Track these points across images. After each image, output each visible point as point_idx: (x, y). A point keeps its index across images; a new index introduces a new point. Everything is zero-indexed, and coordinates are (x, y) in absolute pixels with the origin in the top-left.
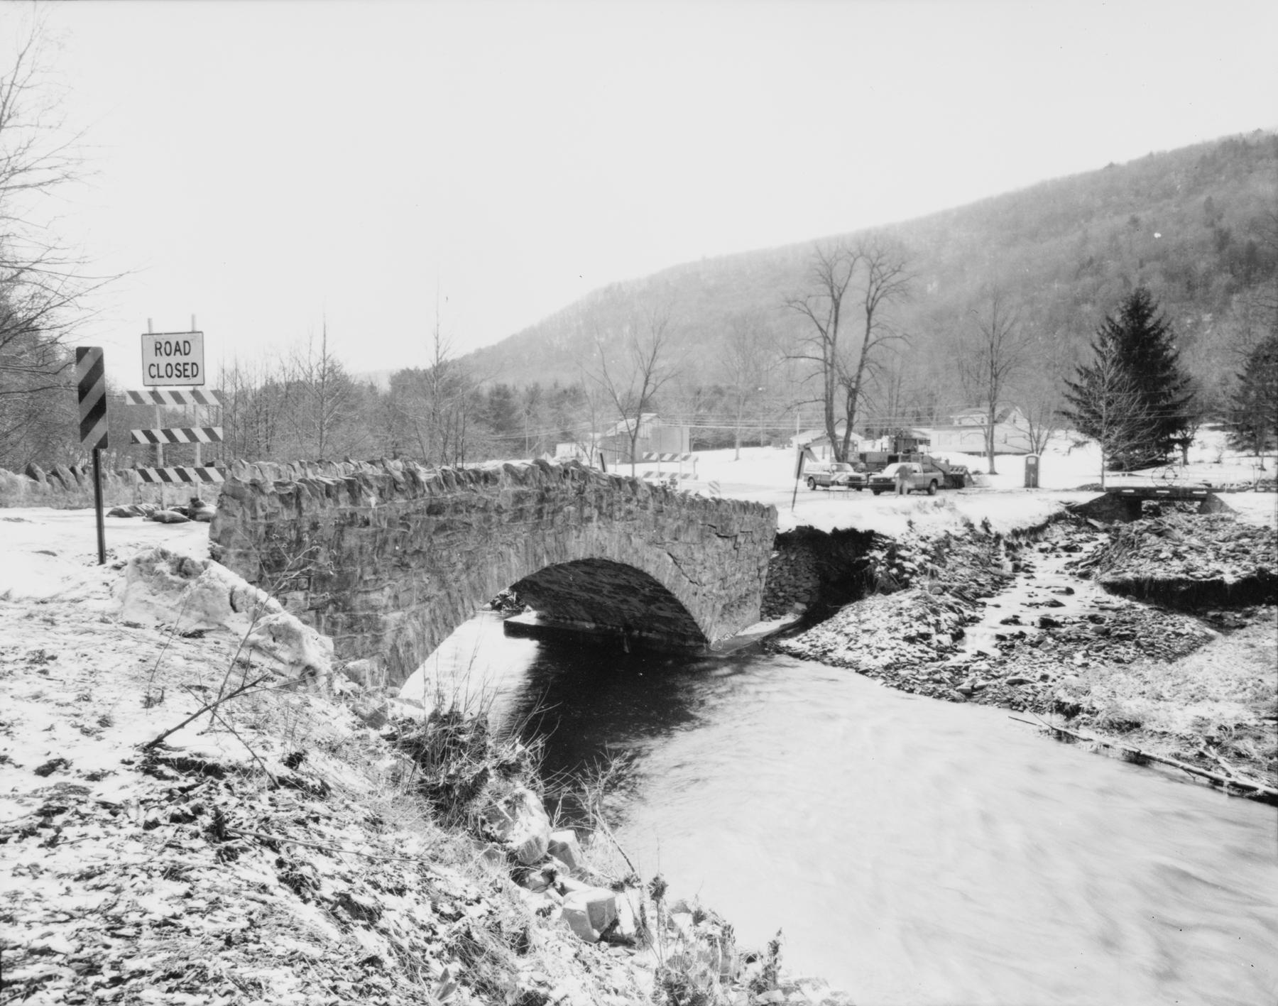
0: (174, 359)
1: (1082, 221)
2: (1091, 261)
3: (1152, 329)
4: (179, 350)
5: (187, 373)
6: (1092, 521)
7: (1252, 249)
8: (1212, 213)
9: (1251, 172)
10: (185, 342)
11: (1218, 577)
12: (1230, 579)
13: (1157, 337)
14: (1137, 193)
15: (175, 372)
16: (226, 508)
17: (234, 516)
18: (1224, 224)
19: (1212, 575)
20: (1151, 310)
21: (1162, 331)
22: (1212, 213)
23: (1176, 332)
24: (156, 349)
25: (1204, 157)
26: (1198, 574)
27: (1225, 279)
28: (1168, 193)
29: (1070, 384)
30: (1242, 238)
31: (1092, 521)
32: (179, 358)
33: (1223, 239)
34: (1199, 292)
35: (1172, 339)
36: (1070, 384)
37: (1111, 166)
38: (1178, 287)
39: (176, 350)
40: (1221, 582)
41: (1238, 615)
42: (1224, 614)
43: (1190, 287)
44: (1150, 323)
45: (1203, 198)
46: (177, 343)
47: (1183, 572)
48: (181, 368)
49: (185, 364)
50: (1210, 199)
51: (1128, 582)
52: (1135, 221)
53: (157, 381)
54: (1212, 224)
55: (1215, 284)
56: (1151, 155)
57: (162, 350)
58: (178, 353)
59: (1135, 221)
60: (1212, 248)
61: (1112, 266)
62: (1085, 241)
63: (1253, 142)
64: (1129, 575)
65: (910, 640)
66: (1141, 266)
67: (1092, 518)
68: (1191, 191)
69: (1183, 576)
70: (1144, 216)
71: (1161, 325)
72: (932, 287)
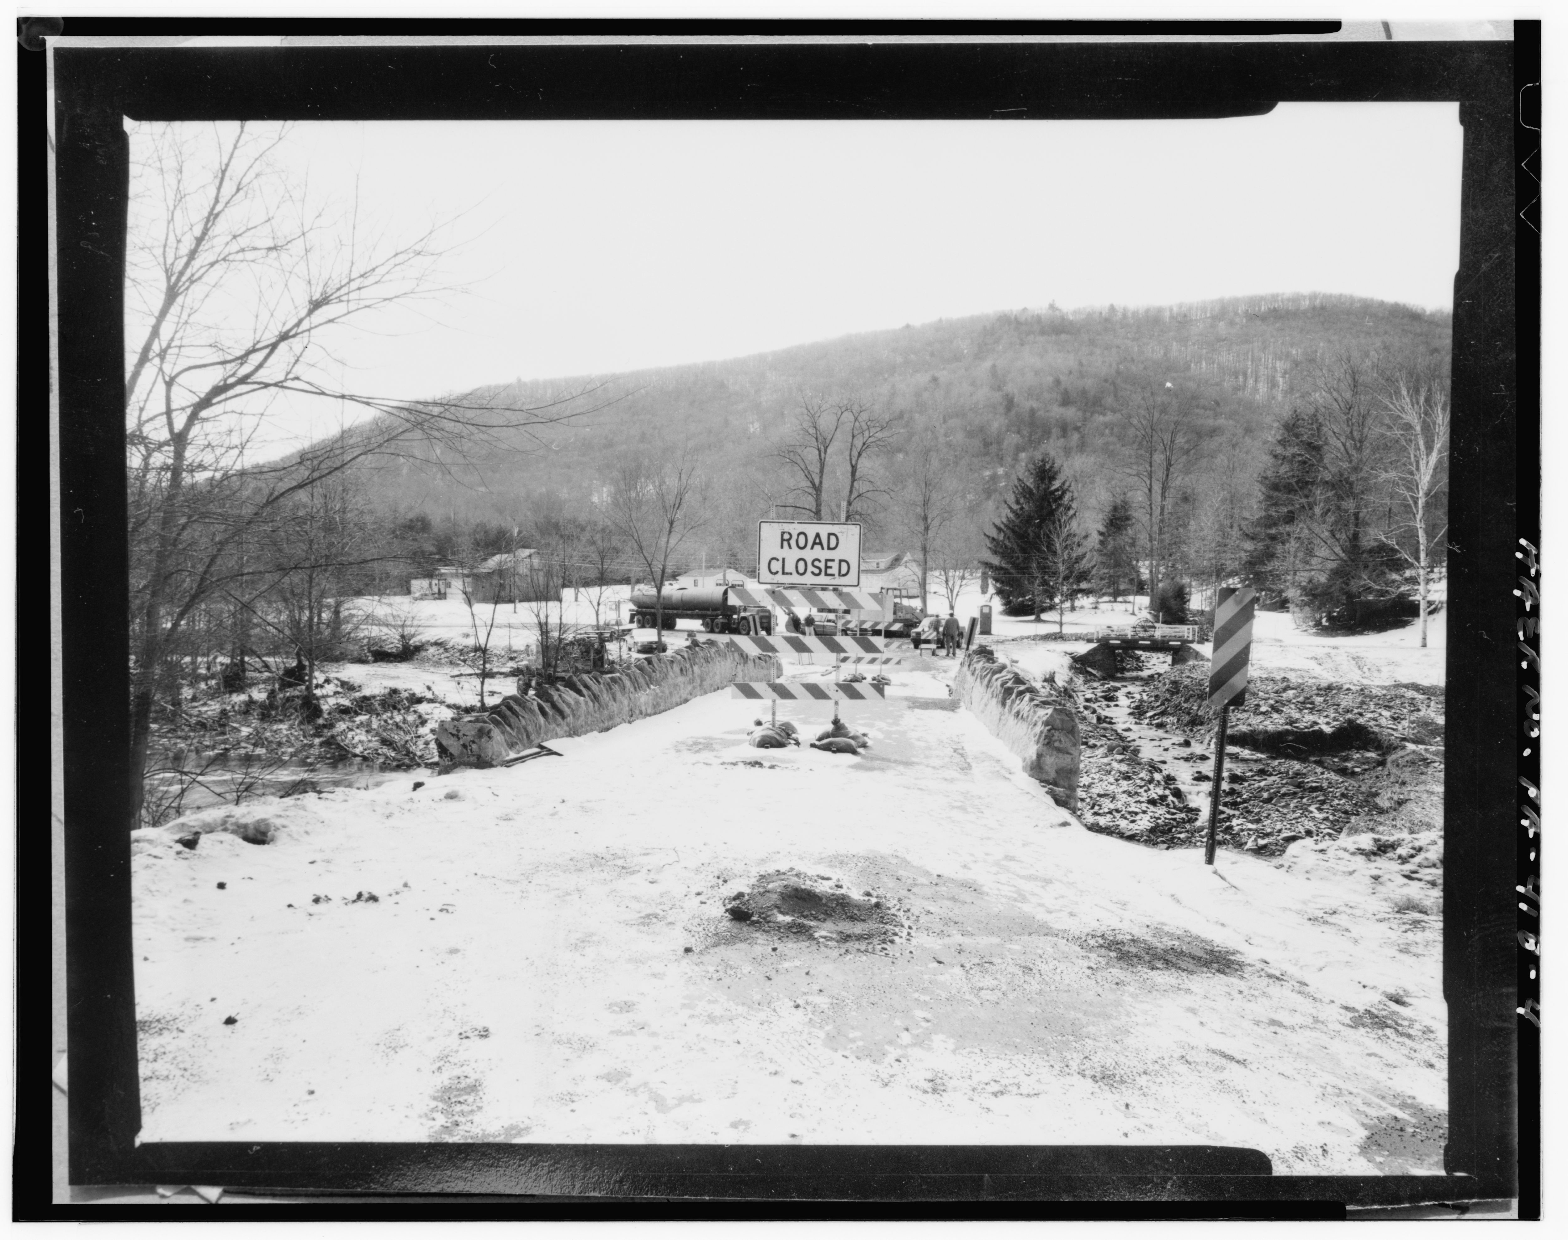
0: (809, 555)
1: (886, 376)
2: (901, 416)
3: (1057, 490)
4: (821, 543)
5: (829, 571)
6: (1089, 669)
7: (1033, 412)
8: (997, 380)
9: (1022, 345)
10: (830, 534)
11: (1316, 728)
12: (1327, 730)
13: (1061, 497)
14: (932, 354)
15: (810, 568)
16: (1057, 744)
17: (1068, 753)
18: (1010, 388)
19: (1312, 726)
20: (1056, 473)
21: (1064, 493)
22: (997, 380)
23: (1076, 494)
24: (783, 540)
25: (985, 328)
26: (1301, 725)
27: (1013, 439)
28: (957, 358)
29: (988, 537)
30: (1026, 404)
31: (1089, 669)
32: (824, 554)
33: (1010, 404)
34: (993, 449)
35: (1072, 500)
36: (988, 537)
37: (908, 326)
38: (977, 443)
39: (814, 543)
40: (1321, 732)
41: (1336, 760)
42: (1324, 758)
43: (987, 444)
44: (1056, 484)
45: (987, 364)
46: (818, 535)
47: (1287, 724)
48: (822, 565)
49: (827, 561)
50: (994, 366)
51: (1245, 734)
52: (935, 379)
53: (780, 578)
54: (999, 389)
55: (1006, 442)
56: (940, 320)
57: (793, 542)
58: (817, 547)
59: (935, 379)
60: (1001, 409)
61: (920, 421)
62: (893, 394)
63: (1022, 319)
64: (1244, 728)
65: (1152, 802)
66: (945, 422)
67: (1090, 666)
68: (982, 350)
69: (1288, 727)
70: (943, 375)
71: (1066, 487)
72: (755, 428)
